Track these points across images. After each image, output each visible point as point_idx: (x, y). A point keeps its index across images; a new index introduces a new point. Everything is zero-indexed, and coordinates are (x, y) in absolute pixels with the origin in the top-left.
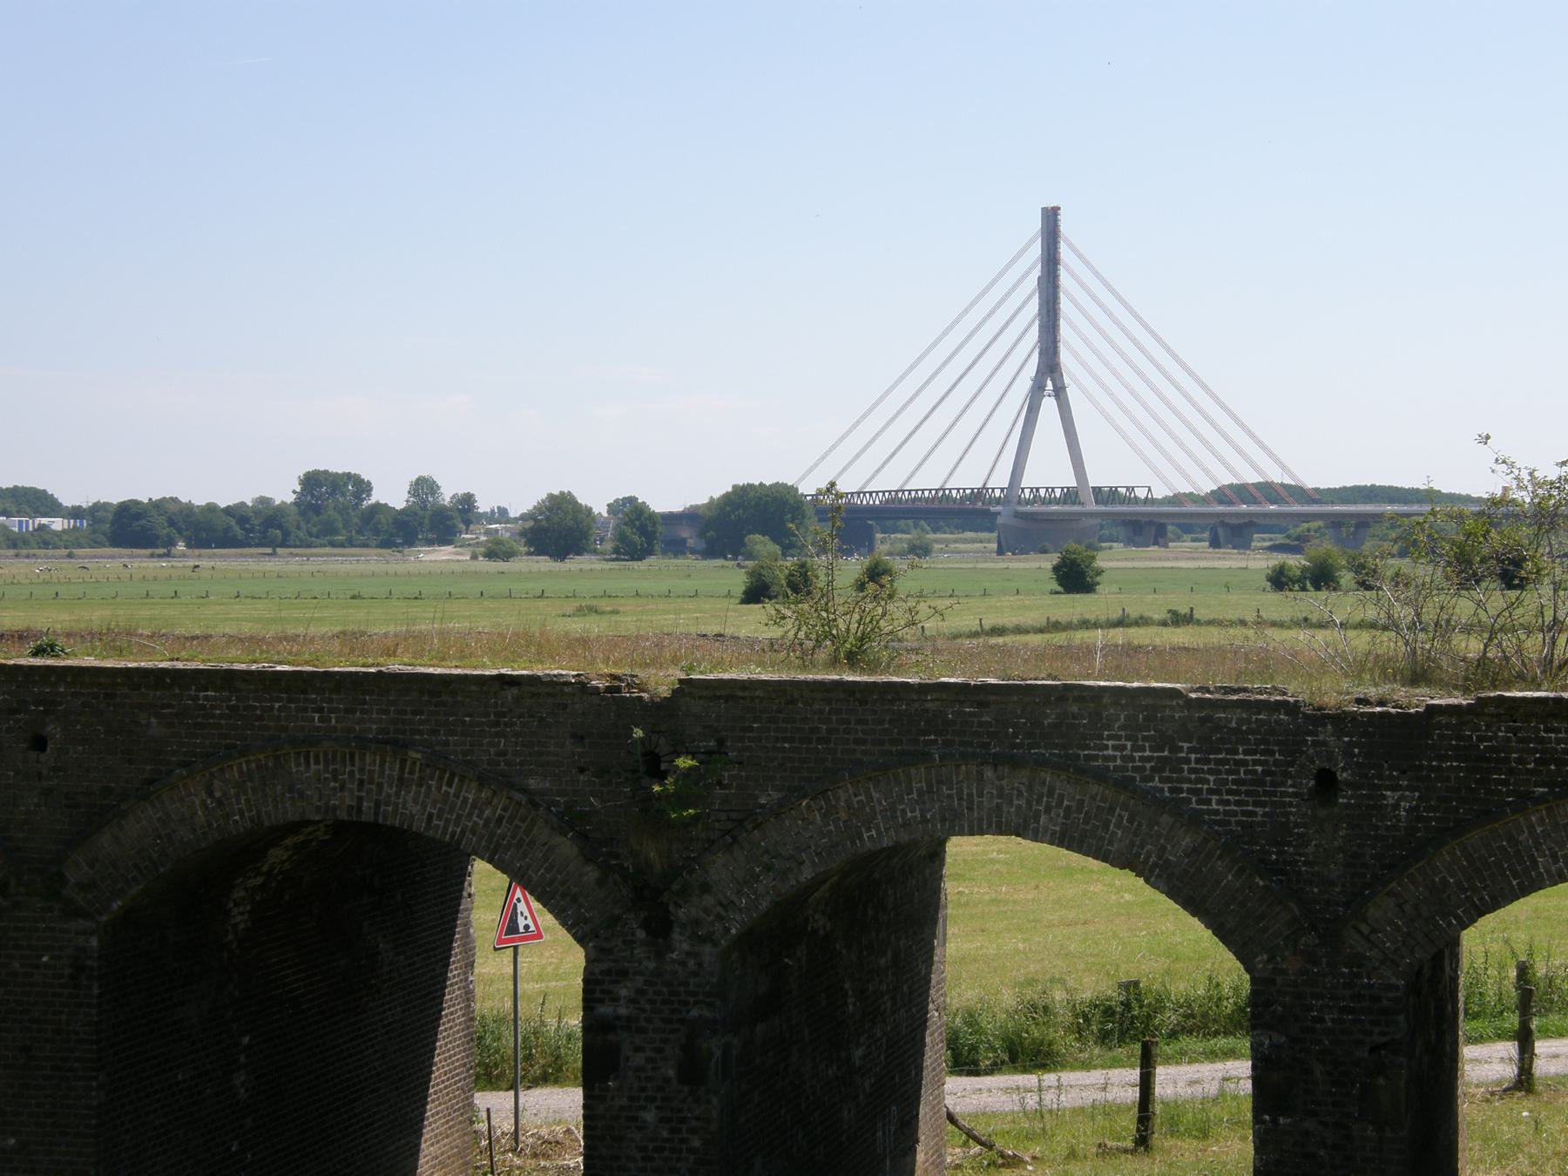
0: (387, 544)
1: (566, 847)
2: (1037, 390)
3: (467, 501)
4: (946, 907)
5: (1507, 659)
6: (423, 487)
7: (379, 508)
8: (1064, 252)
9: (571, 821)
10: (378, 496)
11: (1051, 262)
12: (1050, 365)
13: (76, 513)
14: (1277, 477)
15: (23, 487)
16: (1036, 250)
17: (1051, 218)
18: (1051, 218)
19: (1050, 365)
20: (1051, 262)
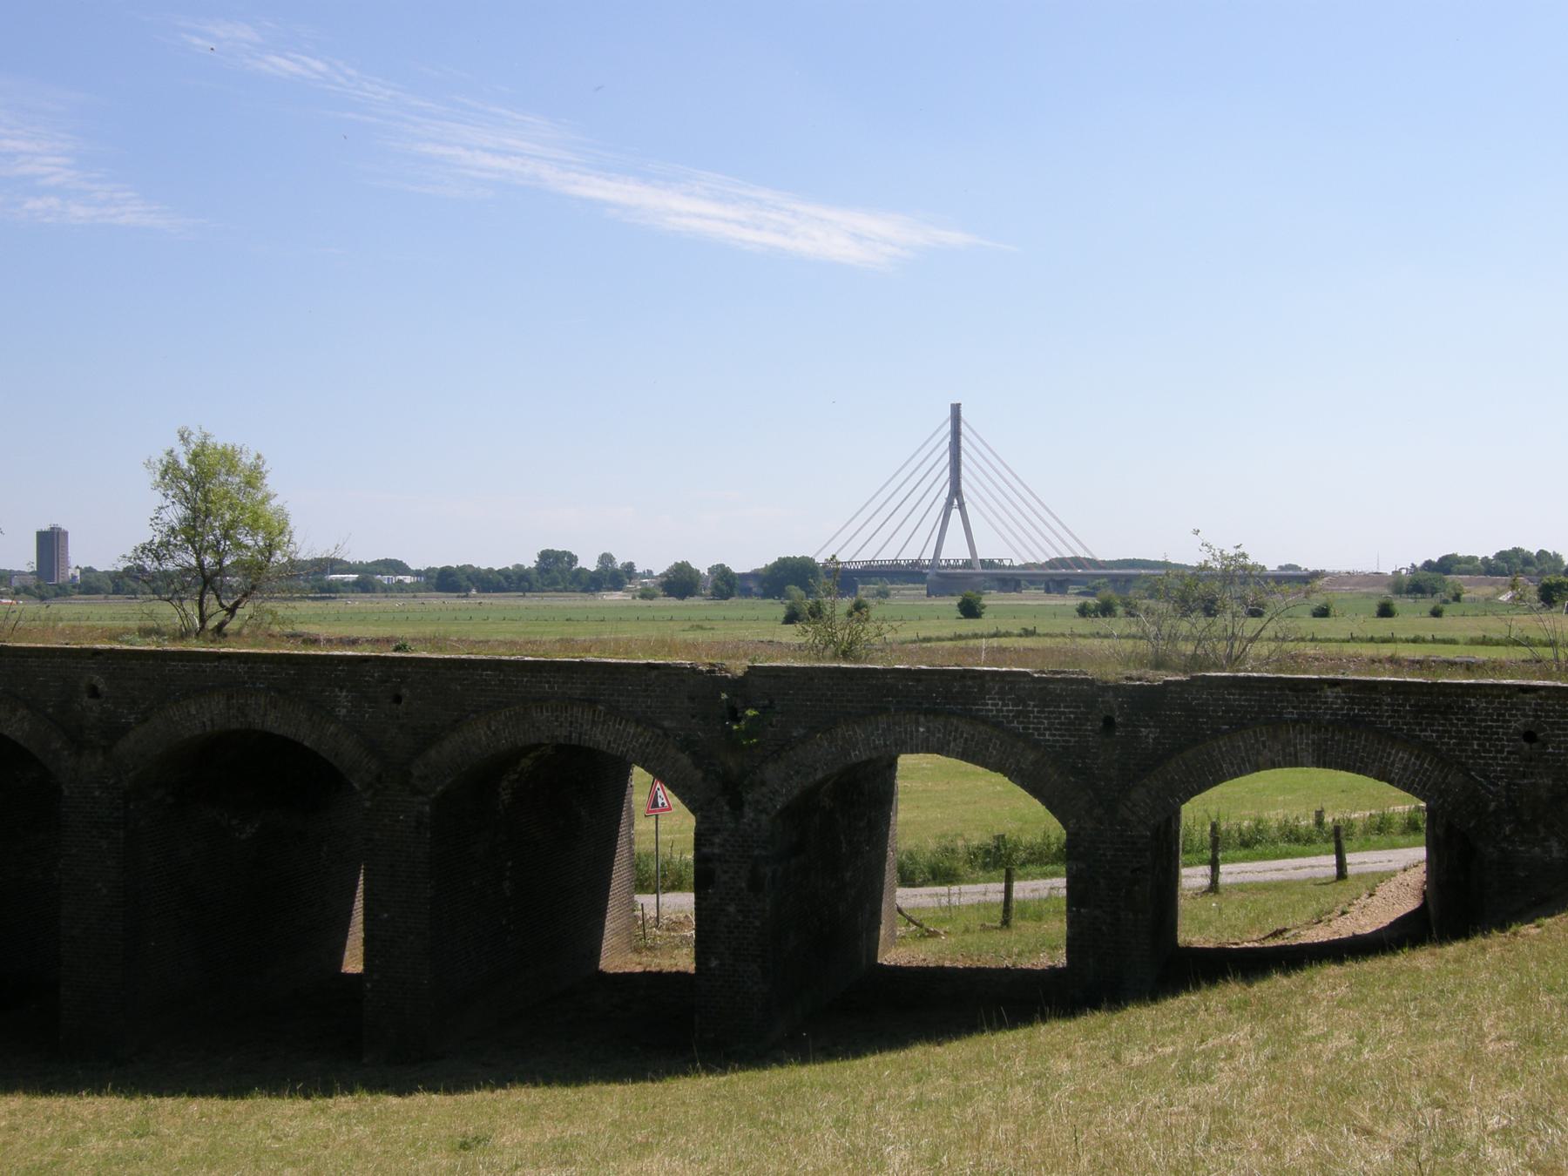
1: (685, 760)
2: (949, 505)
3: (630, 566)
6: (606, 559)
8: (963, 427)
12: (956, 490)
13: (418, 573)
14: (1082, 554)
16: (948, 427)
17: (956, 410)
18: (956, 410)
19: (956, 490)
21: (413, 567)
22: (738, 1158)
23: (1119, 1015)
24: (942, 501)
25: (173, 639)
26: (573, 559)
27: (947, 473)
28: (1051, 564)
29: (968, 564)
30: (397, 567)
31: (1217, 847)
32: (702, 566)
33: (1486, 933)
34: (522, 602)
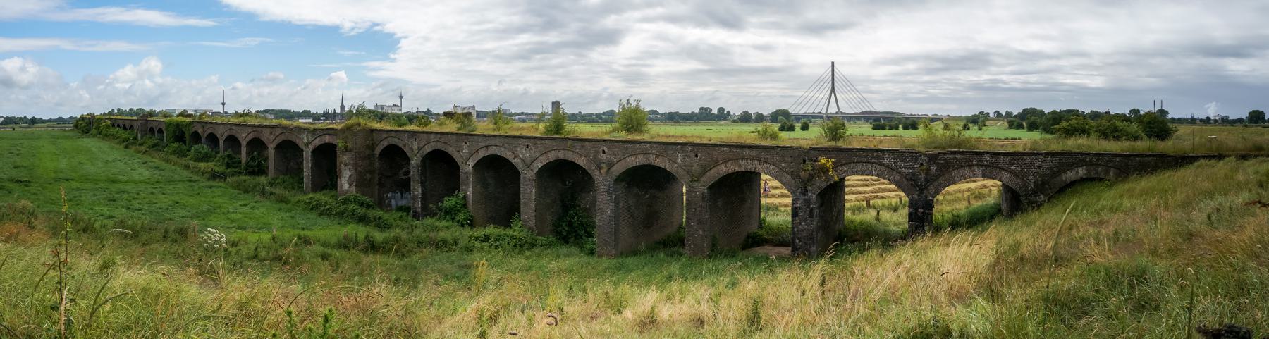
0: (280, 125)
1: (789, 177)
2: (831, 93)
3: (729, 112)
4: (1039, 206)
5: (381, 184)
6: (721, 110)
7: (713, 114)
8: (835, 69)
9: (791, 173)
10: (713, 112)
11: (833, 71)
12: (833, 89)
13: (662, 114)
14: (872, 110)
15: (1031, 108)
16: (830, 69)
17: (833, 63)
18: (833, 63)
19: (833, 89)
20: (833, 71)
21: (660, 112)
22: (652, 318)
23: (1127, 186)
24: (829, 91)
25: (207, 155)
26: (710, 110)
27: (831, 83)
28: (863, 113)
29: (837, 113)
30: (655, 112)
31: (848, 180)
32: (752, 112)
33: (720, 203)
34: (673, 128)
